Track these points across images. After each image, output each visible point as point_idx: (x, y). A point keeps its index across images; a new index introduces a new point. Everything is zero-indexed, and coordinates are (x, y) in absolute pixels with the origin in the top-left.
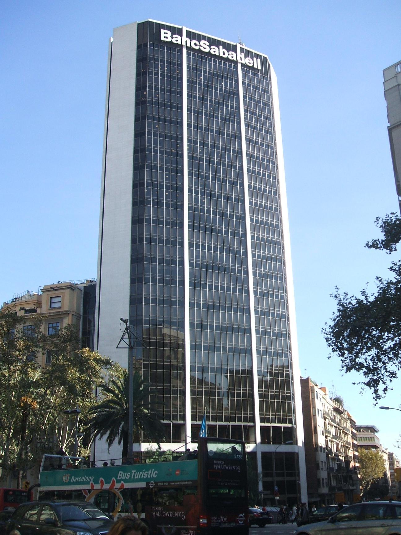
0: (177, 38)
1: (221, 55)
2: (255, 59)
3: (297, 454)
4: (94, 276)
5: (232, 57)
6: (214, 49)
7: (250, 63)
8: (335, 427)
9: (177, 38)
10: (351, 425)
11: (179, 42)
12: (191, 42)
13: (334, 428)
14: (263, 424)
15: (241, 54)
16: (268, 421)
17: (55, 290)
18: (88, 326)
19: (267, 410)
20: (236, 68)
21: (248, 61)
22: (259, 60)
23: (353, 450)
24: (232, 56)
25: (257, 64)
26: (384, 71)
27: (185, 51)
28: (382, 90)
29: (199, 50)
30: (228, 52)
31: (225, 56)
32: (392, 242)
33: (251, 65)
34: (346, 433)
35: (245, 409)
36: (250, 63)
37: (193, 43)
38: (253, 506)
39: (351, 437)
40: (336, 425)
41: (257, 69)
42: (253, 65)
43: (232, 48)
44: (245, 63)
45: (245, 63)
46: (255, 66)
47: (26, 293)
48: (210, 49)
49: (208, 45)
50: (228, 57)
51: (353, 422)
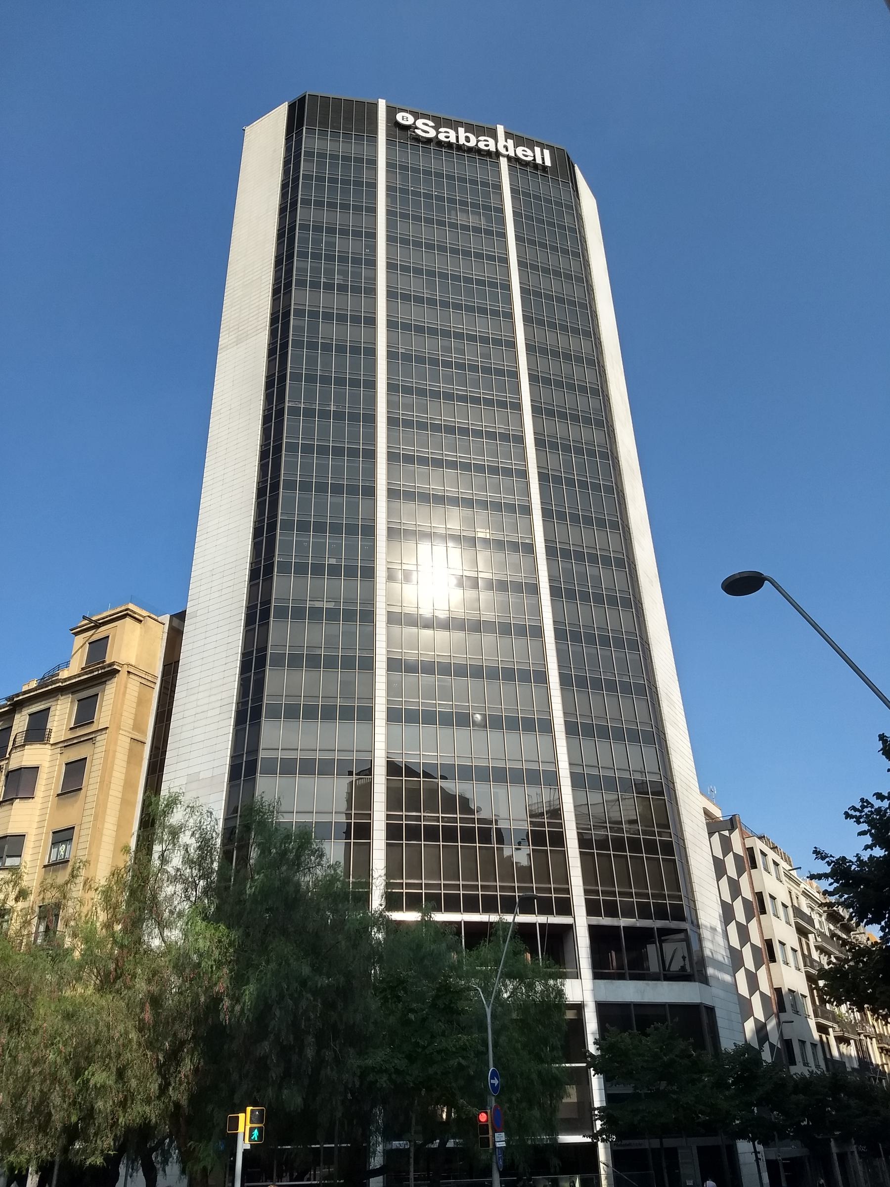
0: (448, 133)
1: (462, 141)
6: (485, 141)
7: (526, 156)
9: (448, 133)
11: (492, 148)
15: (506, 141)
16: (612, 911)
19: (608, 880)
20: (498, 165)
22: (547, 153)
27: (504, 162)
31: (472, 143)
32: (86, 950)
33: (530, 159)
38: (597, 1073)
41: (544, 168)
42: (534, 160)
44: (497, 149)
45: (497, 149)
46: (539, 161)
49: (432, 127)
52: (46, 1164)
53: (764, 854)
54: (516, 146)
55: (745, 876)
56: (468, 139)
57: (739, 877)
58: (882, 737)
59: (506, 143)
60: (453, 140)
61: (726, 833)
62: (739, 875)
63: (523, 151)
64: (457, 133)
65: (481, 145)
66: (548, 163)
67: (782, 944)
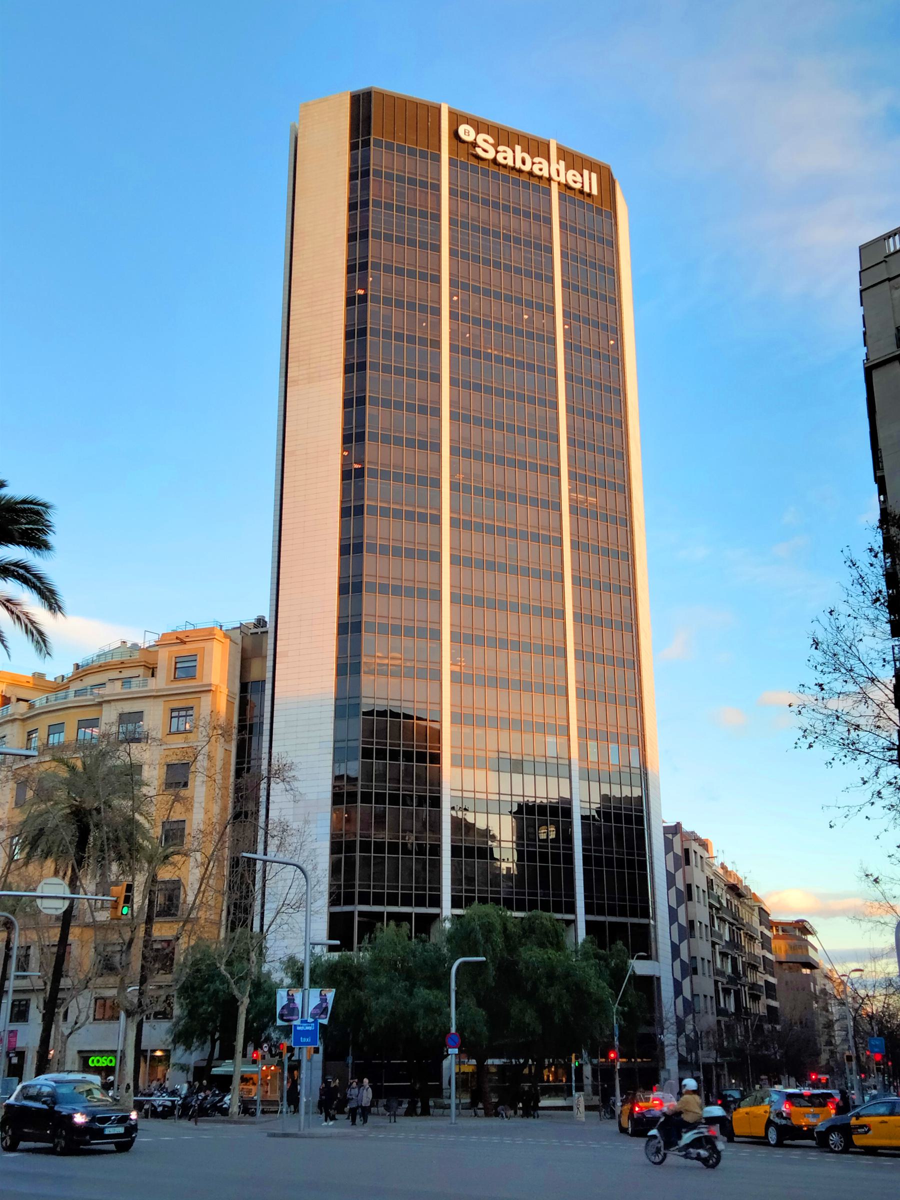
1: (519, 164)
2: (586, 173)
3: (659, 979)
4: (266, 613)
5: (541, 170)
7: (575, 182)
8: (730, 923)
10: (760, 920)
12: (566, 174)
13: (727, 925)
14: (592, 918)
15: (558, 163)
16: (601, 912)
17: (184, 643)
18: (11, 890)
20: (548, 193)
21: (572, 177)
22: (594, 176)
23: (764, 972)
24: (540, 167)
25: (590, 183)
26: (861, 248)
28: (857, 287)
29: (531, 174)
30: (532, 158)
31: (527, 168)
33: (578, 186)
34: (751, 936)
35: (545, 886)
36: (575, 182)
37: (572, 177)
39: (760, 944)
40: (731, 920)
42: (583, 187)
43: (538, 148)
44: (566, 181)
45: (566, 181)
46: (586, 189)
47: (119, 644)
48: (497, 152)
49: (492, 145)
50: (531, 169)
51: (763, 913)
52: (377, 1104)
53: (695, 852)
54: (567, 170)
55: (683, 907)
56: (524, 163)
57: (682, 980)
58: (897, 328)
59: (557, 166)
60: (510, 162)
61: (670, 836)
62: (676, 870)
63: (574, 175)
64: (514, 152)
65: (536, 171)
66: (595, 192)
67: (698, 887)
